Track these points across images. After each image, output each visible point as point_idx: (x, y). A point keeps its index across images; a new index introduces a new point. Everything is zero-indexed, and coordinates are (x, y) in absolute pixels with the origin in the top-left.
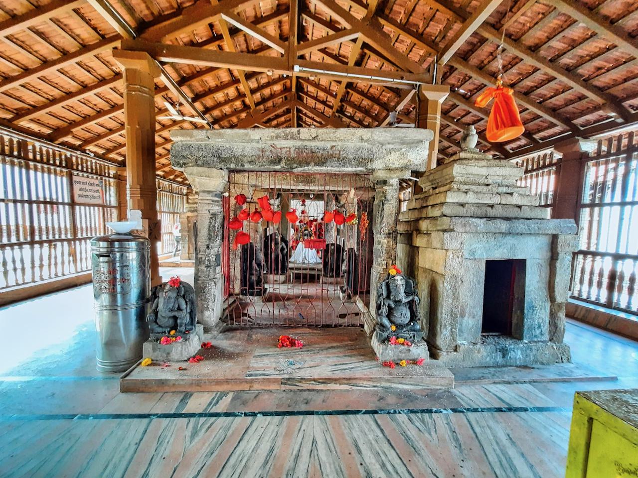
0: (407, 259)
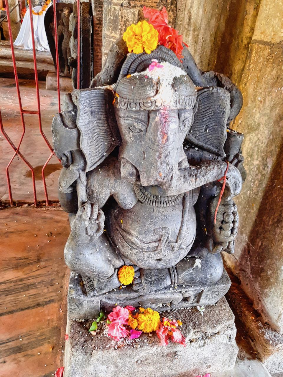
0: (213, 22)
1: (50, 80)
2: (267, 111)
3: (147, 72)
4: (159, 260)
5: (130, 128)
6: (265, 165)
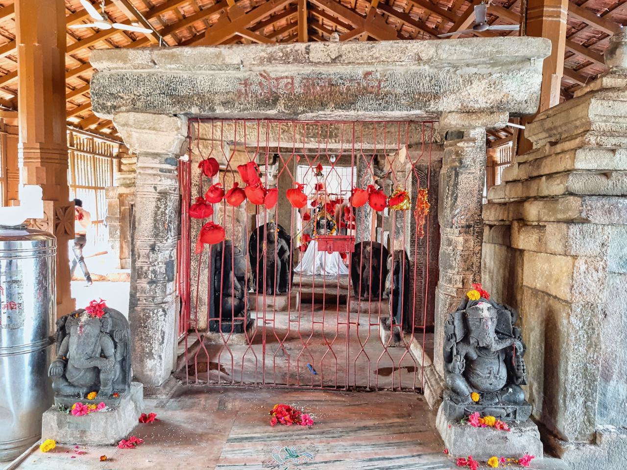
0: (501, 271)
1: (352, 304)
2: (536, 320)
3: (477, 306)
4: (491, 384)
5: (474, 324)
6: (541, 347)
